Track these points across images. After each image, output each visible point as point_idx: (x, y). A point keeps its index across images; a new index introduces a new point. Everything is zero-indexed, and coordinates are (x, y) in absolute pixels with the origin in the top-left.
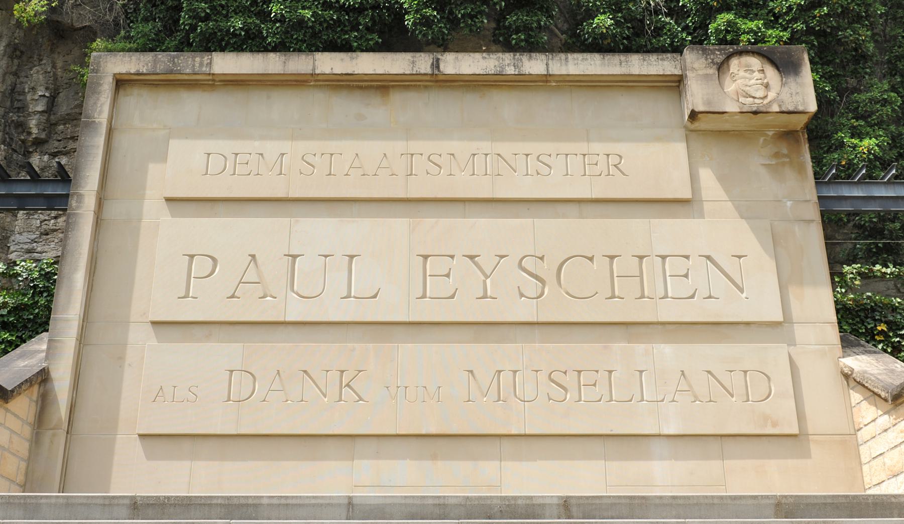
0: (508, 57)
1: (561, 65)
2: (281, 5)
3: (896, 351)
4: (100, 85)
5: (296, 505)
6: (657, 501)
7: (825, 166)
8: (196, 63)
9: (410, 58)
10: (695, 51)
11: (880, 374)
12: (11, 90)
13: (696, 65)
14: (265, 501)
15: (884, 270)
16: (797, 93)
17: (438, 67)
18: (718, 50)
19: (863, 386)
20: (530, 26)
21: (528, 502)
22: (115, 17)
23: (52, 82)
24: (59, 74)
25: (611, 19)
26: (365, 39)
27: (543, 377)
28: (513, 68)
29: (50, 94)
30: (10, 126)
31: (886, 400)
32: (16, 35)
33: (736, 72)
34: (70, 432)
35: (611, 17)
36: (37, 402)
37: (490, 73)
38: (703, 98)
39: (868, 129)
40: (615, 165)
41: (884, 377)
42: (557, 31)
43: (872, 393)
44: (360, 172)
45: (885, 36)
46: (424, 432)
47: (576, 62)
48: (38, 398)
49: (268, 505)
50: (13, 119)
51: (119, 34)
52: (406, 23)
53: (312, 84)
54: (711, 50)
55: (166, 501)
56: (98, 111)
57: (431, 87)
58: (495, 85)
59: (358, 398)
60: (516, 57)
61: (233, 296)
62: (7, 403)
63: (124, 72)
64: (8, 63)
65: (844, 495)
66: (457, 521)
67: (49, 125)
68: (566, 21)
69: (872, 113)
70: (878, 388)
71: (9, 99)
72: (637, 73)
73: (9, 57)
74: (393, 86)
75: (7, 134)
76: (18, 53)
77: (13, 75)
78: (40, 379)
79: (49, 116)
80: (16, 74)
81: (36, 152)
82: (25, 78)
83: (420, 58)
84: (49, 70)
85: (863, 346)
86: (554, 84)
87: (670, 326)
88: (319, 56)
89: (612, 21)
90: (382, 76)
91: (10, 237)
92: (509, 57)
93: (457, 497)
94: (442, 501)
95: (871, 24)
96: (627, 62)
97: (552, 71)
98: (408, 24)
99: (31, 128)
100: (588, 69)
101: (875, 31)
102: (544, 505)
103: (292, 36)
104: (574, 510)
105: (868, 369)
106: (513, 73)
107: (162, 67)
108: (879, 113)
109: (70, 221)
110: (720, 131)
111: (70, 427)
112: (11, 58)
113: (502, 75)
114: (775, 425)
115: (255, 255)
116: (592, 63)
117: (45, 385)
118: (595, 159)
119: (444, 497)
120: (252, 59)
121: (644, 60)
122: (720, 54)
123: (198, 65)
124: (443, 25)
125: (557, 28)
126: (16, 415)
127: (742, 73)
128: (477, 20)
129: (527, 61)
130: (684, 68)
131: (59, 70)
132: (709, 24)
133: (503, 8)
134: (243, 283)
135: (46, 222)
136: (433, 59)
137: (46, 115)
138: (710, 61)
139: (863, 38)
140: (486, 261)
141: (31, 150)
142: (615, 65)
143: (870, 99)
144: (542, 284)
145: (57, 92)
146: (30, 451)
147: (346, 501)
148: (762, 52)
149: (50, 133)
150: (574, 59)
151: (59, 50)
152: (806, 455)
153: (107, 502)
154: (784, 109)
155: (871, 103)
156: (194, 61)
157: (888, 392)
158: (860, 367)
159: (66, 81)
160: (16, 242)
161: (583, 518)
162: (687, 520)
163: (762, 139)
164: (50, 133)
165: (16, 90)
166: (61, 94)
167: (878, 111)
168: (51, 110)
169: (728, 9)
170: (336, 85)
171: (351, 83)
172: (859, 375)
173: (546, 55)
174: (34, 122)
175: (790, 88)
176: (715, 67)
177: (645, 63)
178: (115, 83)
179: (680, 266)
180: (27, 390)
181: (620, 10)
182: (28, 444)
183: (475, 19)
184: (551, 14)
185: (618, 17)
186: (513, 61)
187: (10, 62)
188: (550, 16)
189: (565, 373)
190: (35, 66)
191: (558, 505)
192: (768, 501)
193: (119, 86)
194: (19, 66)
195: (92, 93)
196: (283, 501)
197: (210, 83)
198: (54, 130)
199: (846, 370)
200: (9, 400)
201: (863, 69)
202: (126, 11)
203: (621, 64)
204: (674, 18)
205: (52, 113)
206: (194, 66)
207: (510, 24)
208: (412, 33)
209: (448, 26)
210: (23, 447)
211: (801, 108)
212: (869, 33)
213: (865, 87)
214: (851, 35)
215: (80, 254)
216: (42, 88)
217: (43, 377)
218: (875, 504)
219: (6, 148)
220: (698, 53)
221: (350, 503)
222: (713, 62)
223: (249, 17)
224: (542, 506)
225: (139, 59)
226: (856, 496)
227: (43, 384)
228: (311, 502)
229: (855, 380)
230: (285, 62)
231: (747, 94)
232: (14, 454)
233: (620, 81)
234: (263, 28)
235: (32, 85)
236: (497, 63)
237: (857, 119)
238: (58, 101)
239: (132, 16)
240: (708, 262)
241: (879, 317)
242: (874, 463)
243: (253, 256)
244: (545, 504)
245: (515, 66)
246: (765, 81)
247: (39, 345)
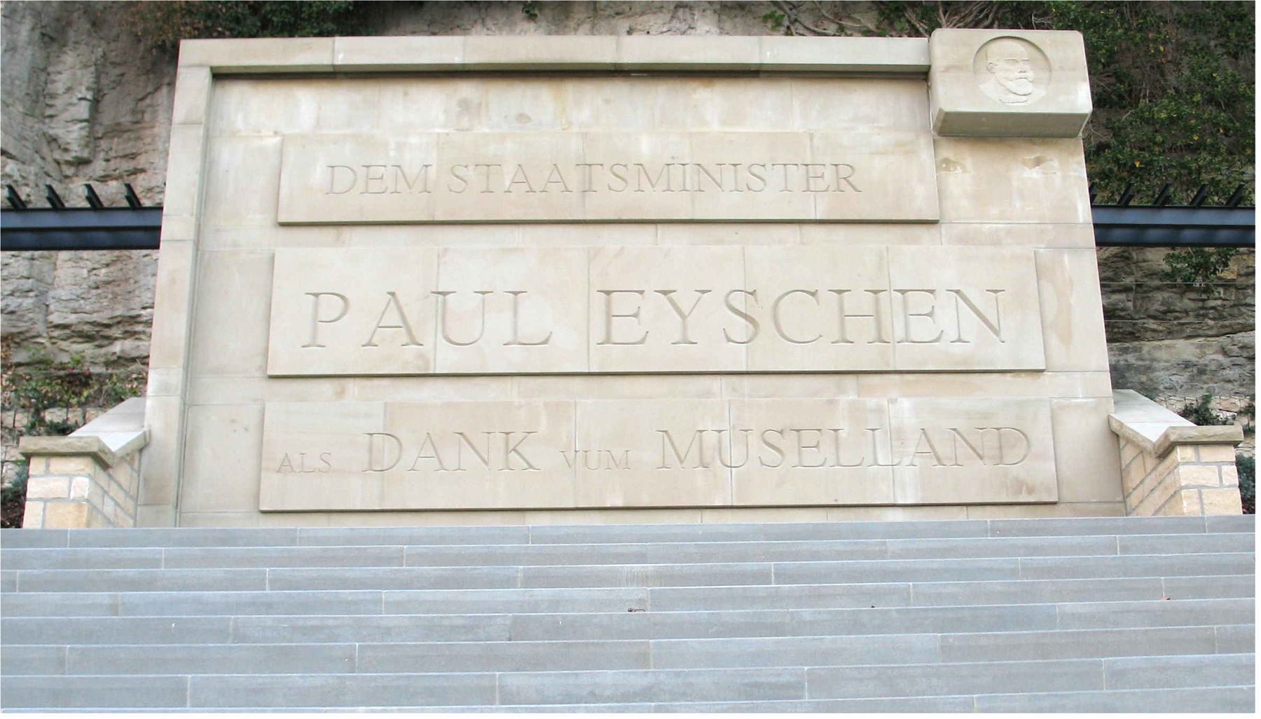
27: (753, 439)
44: (525, 187)
59: (526, 466)
91: (47, 292)
114: (1031, 491)
118: (820, 170)
135: (94, 272)
140: (685, 300)
144: (754, 327)
145: (102, 94)
166: (106, 96)
189: (781, 432)
199: (1115, 426)
216: (83, 89)
240: (958, 297)
243: (393, 294)
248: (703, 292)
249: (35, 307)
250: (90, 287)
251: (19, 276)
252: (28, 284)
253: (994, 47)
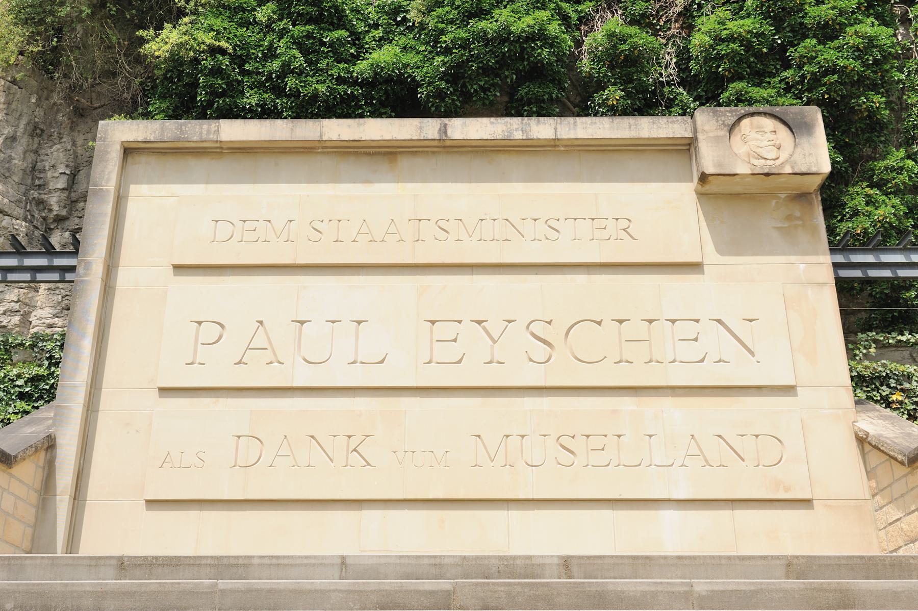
0: (515, 122)
1: (570, 129)
2: (296, 80)
3: (912, 417)
4: (107, 153)
5: (288, 565)
6: (662, 561)
7: (839, 235)
8: (203, 130)
9: (418, 124)
10: (706, 113)
11: (896, 438)
12: (32, 167)
13: (706, 128)
14: (256, 561)
15: (900, 337)
16: (810, 154)
17: (445, 133)
18: (730, 112)
19: (879, 449)
20: (541, 98)
21: (527, 561)
22: (133, 95)
23: (73, 160)
24: (79, 152)
25: (622, 90)
26: (378, 113)
28: (520, 132)
29: (71, 171)
30: (31, 203)
31: (902, 463)
32: (36, 113)
33: (747, 133)
34: (77, 498)
35: (621, 88)
36: (43, 468)
37: (498, 137)
38: (713, 161)
39: (884, 197)
40: (624, 230)
41: (901, 440)
42: (569, 104)
43: (888, 457)
45: (901, 104)
46: (431, 497)
47: (584, 125)
48: (44, 464)
49: (259, 565)
50: (34, 196)
51: (137, 110)
52: (419, 96)
53: (319, 150)
54: (722, 112)
55: (154, 561)
56: (105, 179)
57: (439, 152)
58: (504, 150)
60: (524, 122)
61: (239, 363)
62: (10, 468)
63: (132, 140)
64: (28, 141)
65: (859, 556)
66: (452, 581)
67: (70, 202)
68: (579, 94)
69: (888, 181)
70: (894, 452)
71: (30, 177)
72: (647, 137)
73: (29, 135)
74: (401, 153)
75: (28, 211)
76: (38, 131)
77: (34, 153)
78: (46, 445)
79: (70, 193)
80: (36, 152)
81: (58, 228)
82: (46, 157)
83: (428, 124)
84: (69, 148)
85: (878, 411)
86: (563, 149)
87: (680, 390)
88: (326, 122)
89: (623, 93)
90: (390, 142)
91: (31, 312)
92: (517, 122)
93: (454, 556)
94: (438, 561)
95: (887, 91)
96: (636, 125)
97: (560, 135)
98: (421, 97)
99: (51, 205)
100: (596, 133)
101: (891, 99)
102: (543, 565)
103: (307, 109)
104: (575, 570)
105: (882, 432)
106: (521, 138)
107: (170, 135)
108: (895, 181)
109: (78, 288)
110: (731, 194)
111: (77, 493)
112: (32, 136)
113: (510, 140)
114: (787, 490)
115: (262, 321)
116: (601, 127)
117: (52, 451)
118: (603, 223)
119: (440, 557)
120: (259, 126)
121: (654, 123)
122: (732, 116)
123: (205, 132)
124: (455, 98)
125: (569, 101)
126: (20, 481)
127: (753, 135)
128: (489, 94)
129: (535, 126)
130: (695, 131)
131: (79, 148)
132: (722, 93)
133: (514, 80)
134: (250, 349)
135: (67, 298)
136: (441, 124)
137: (67, 192)
138: (721, 122)
139: (878, 105)
140: (495, 327)
141: (52, 227)
142: (625, 129)
143: (885, 167)
145: (78, 170)
146: (36, 517)
147: (339, 561)
148: (774, 114)
149: (71, 210)
150: (583, 123)
151: (79, 128)
152: (796, 395)
153: (93, 563)
154: (797, 171)
155: (887, 171)
156: (202, 128)
157: (904, 455)
158: (876, 431)
159: (86, 159)
160: (38, 317)
161: (585, 578)
162: (693, 580)
163: (774, 202)
164: (71, 210)
165: (36, 168)
167: (894, 179)
168: (72, 187)
169: (741, 78)
170: (344, 152)
171: (359, 150)
172: (874, 438)
173: (555, 120)
174: (55, 199)
175: (803, 149)
176: (726, 128)
177: (655, 126)
178: (122, 151)
179: (690, 330)
180: (32, 455)
181: (631, 81)
182: (34, 510)
183: (487, 92)
184: (562, 86)
185: (629, 88)
186: (521, 125)
187: (31, 140)
188: (561, 88)
190: (55, 144)
191: (558, 565)
192: (778, 562)
193: (127, 155)
194: (39, 144)
195: (100, 161)
196: (274, 561)
197: (218, 150)
198: (75, 207)
199: (861, 434)
200: (13, 466)
201: (878, 137)
202: (143, 88)
203: (630, 128)
204: (687, 89)
205: (72, 190)
206: (201, 133)
207: (522, 97)
208: (425, 106)
209: (461, 99)
210: (29, 513)
211: (814, 170)
212: (883, 99)
213: (880, 155)
214: (864, 103)
215: (88, 321)
217: (50, 444)
218: (893, 565)
219: (27, 224)
220: (709, 114)
221: (343, 563)
222: (724, 124)
223: (264, 92)
224: (542, 566)
225: (147, 127)
226: (873, 557)
227: (49, 450)
228: (303, 562)
229: (870, 444)
230: (292, 129)
231: (759, 155)
232: (20, 521)
233: (633, 145)
234: (278, 103)
235: (53, 163)
236: (505, 128)
237: (871, 186)
238: (78, 178)
239: (150, 93)
241: (895, 385)
242: (890, 528)
244: (545, 564)
245: (523, 131)
246: (778, 142)
247: (46, 412)
248: (510, 321)
249: (21, 322)
250: (63, 309)
251: (10, 301)
252: (16, 306)
253: (746, 122)
